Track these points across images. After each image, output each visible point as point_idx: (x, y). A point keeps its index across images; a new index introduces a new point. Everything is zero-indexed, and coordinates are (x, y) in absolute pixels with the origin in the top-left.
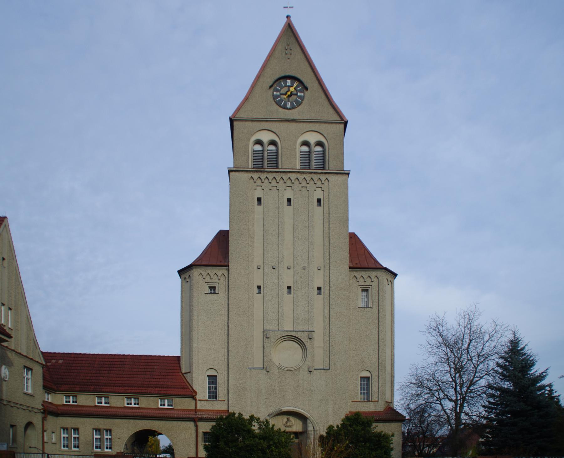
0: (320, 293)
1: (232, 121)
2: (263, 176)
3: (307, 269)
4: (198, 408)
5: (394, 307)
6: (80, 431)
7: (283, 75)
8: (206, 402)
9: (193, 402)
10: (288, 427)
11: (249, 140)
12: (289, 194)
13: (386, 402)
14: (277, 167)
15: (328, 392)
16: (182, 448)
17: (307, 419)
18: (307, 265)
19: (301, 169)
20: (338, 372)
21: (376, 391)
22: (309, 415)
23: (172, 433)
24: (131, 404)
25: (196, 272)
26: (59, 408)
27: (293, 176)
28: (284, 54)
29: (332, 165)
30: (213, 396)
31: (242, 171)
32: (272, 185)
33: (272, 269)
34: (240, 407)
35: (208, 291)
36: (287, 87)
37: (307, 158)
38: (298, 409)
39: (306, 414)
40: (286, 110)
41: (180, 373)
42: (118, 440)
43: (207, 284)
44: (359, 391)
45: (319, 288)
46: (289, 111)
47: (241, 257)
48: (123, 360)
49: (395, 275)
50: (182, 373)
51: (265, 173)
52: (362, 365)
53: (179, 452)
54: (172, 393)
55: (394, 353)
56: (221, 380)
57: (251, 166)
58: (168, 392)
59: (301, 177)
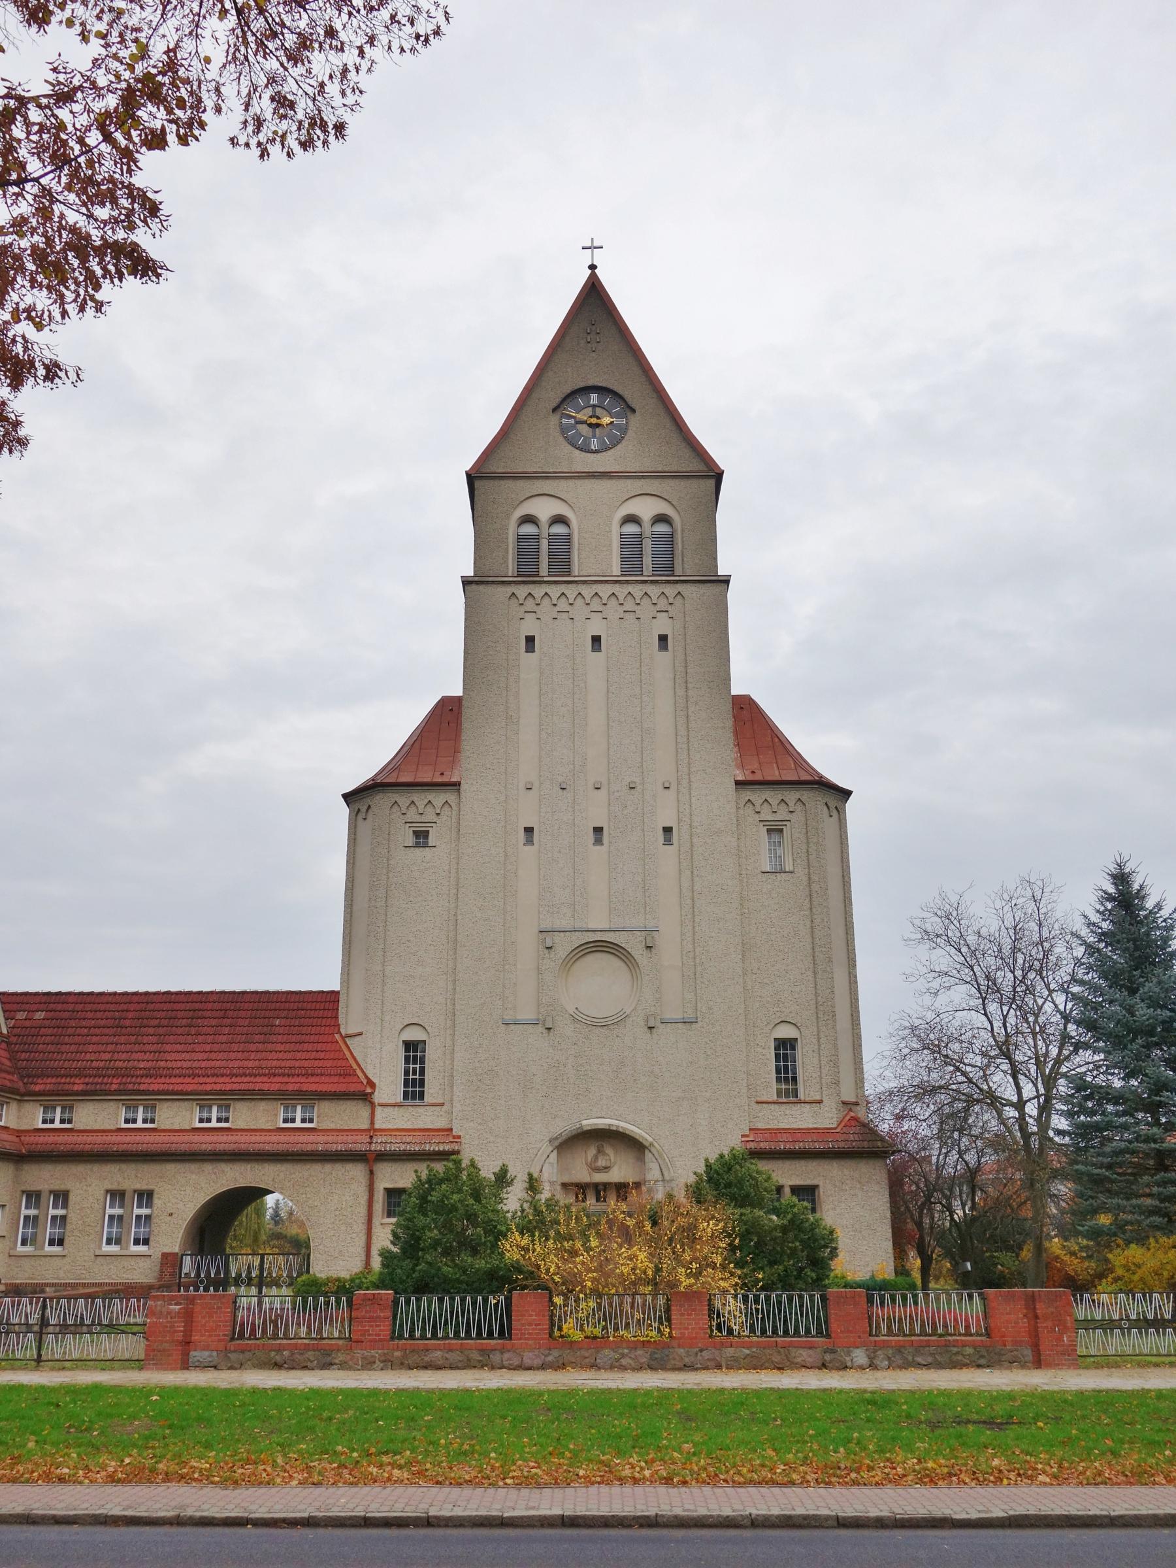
0: (668, 841)
1: (471, 478)
2: (538, 591)
3: (639, 788)
4: (377, 1126)
5: (848, 867)
6: (72, 1198)
7: (582, 385)
8: (396, 1108)
9: (365, 1112)
10: (597, 1170)
11: (508, 517)
12: (596, 627)
13: (844, 1103)
14: (569, 572)
15: (697, 1078)
16: (332, 1233)
17: (647, 1152)
18: (637, 780)
19: (622, 575)
20: (718, 1028)
21: (814, 1075)
22: (650, 1139)
23: (308, 1196)
24: (52, 1121)
25: (381, 802)
26: (26, 1139)
27: (605, 591)
28: (583, 342)
29: (686, 565)
30: (414, 1089)
31: (493, 582)
32: (557, 608)
33: (558, 789)
34: (480, 1121)
35: (410, 840)
36: (590, 409)
37: (632, 550)
38: (622, 1124)
39: (643, 1137)
40: (589, 455)
41: (337, 1036)
42: (170, 1218)
43: (408, 825)
44: (774, 1075)
45: (668, 830)
46: (595, 455)
47: (488, 766)
48: (197, 1006)
49: (847, 794)
50: (341, 1035)
51: (543, 586)
52: (776, 1009)
53: (321, 1247)
54: (313, 1087)
55: (856, 977)
56: (432, 1054)
57: (513, 573)
58: (305, 1088)
59: (621, 591)
